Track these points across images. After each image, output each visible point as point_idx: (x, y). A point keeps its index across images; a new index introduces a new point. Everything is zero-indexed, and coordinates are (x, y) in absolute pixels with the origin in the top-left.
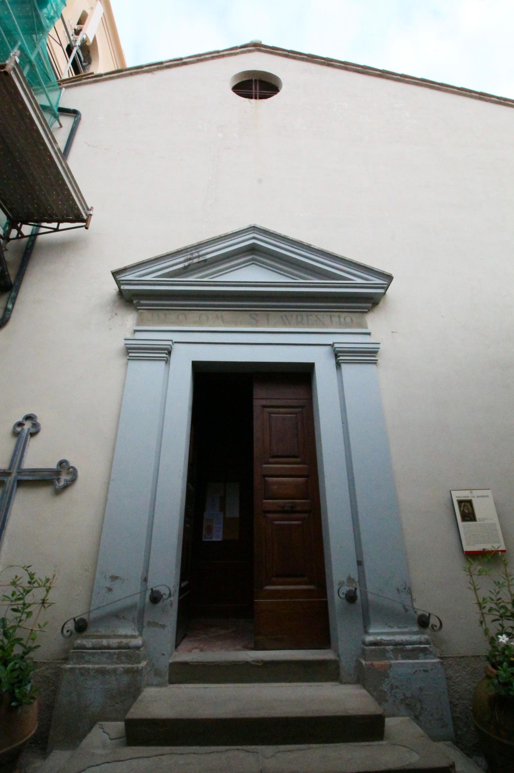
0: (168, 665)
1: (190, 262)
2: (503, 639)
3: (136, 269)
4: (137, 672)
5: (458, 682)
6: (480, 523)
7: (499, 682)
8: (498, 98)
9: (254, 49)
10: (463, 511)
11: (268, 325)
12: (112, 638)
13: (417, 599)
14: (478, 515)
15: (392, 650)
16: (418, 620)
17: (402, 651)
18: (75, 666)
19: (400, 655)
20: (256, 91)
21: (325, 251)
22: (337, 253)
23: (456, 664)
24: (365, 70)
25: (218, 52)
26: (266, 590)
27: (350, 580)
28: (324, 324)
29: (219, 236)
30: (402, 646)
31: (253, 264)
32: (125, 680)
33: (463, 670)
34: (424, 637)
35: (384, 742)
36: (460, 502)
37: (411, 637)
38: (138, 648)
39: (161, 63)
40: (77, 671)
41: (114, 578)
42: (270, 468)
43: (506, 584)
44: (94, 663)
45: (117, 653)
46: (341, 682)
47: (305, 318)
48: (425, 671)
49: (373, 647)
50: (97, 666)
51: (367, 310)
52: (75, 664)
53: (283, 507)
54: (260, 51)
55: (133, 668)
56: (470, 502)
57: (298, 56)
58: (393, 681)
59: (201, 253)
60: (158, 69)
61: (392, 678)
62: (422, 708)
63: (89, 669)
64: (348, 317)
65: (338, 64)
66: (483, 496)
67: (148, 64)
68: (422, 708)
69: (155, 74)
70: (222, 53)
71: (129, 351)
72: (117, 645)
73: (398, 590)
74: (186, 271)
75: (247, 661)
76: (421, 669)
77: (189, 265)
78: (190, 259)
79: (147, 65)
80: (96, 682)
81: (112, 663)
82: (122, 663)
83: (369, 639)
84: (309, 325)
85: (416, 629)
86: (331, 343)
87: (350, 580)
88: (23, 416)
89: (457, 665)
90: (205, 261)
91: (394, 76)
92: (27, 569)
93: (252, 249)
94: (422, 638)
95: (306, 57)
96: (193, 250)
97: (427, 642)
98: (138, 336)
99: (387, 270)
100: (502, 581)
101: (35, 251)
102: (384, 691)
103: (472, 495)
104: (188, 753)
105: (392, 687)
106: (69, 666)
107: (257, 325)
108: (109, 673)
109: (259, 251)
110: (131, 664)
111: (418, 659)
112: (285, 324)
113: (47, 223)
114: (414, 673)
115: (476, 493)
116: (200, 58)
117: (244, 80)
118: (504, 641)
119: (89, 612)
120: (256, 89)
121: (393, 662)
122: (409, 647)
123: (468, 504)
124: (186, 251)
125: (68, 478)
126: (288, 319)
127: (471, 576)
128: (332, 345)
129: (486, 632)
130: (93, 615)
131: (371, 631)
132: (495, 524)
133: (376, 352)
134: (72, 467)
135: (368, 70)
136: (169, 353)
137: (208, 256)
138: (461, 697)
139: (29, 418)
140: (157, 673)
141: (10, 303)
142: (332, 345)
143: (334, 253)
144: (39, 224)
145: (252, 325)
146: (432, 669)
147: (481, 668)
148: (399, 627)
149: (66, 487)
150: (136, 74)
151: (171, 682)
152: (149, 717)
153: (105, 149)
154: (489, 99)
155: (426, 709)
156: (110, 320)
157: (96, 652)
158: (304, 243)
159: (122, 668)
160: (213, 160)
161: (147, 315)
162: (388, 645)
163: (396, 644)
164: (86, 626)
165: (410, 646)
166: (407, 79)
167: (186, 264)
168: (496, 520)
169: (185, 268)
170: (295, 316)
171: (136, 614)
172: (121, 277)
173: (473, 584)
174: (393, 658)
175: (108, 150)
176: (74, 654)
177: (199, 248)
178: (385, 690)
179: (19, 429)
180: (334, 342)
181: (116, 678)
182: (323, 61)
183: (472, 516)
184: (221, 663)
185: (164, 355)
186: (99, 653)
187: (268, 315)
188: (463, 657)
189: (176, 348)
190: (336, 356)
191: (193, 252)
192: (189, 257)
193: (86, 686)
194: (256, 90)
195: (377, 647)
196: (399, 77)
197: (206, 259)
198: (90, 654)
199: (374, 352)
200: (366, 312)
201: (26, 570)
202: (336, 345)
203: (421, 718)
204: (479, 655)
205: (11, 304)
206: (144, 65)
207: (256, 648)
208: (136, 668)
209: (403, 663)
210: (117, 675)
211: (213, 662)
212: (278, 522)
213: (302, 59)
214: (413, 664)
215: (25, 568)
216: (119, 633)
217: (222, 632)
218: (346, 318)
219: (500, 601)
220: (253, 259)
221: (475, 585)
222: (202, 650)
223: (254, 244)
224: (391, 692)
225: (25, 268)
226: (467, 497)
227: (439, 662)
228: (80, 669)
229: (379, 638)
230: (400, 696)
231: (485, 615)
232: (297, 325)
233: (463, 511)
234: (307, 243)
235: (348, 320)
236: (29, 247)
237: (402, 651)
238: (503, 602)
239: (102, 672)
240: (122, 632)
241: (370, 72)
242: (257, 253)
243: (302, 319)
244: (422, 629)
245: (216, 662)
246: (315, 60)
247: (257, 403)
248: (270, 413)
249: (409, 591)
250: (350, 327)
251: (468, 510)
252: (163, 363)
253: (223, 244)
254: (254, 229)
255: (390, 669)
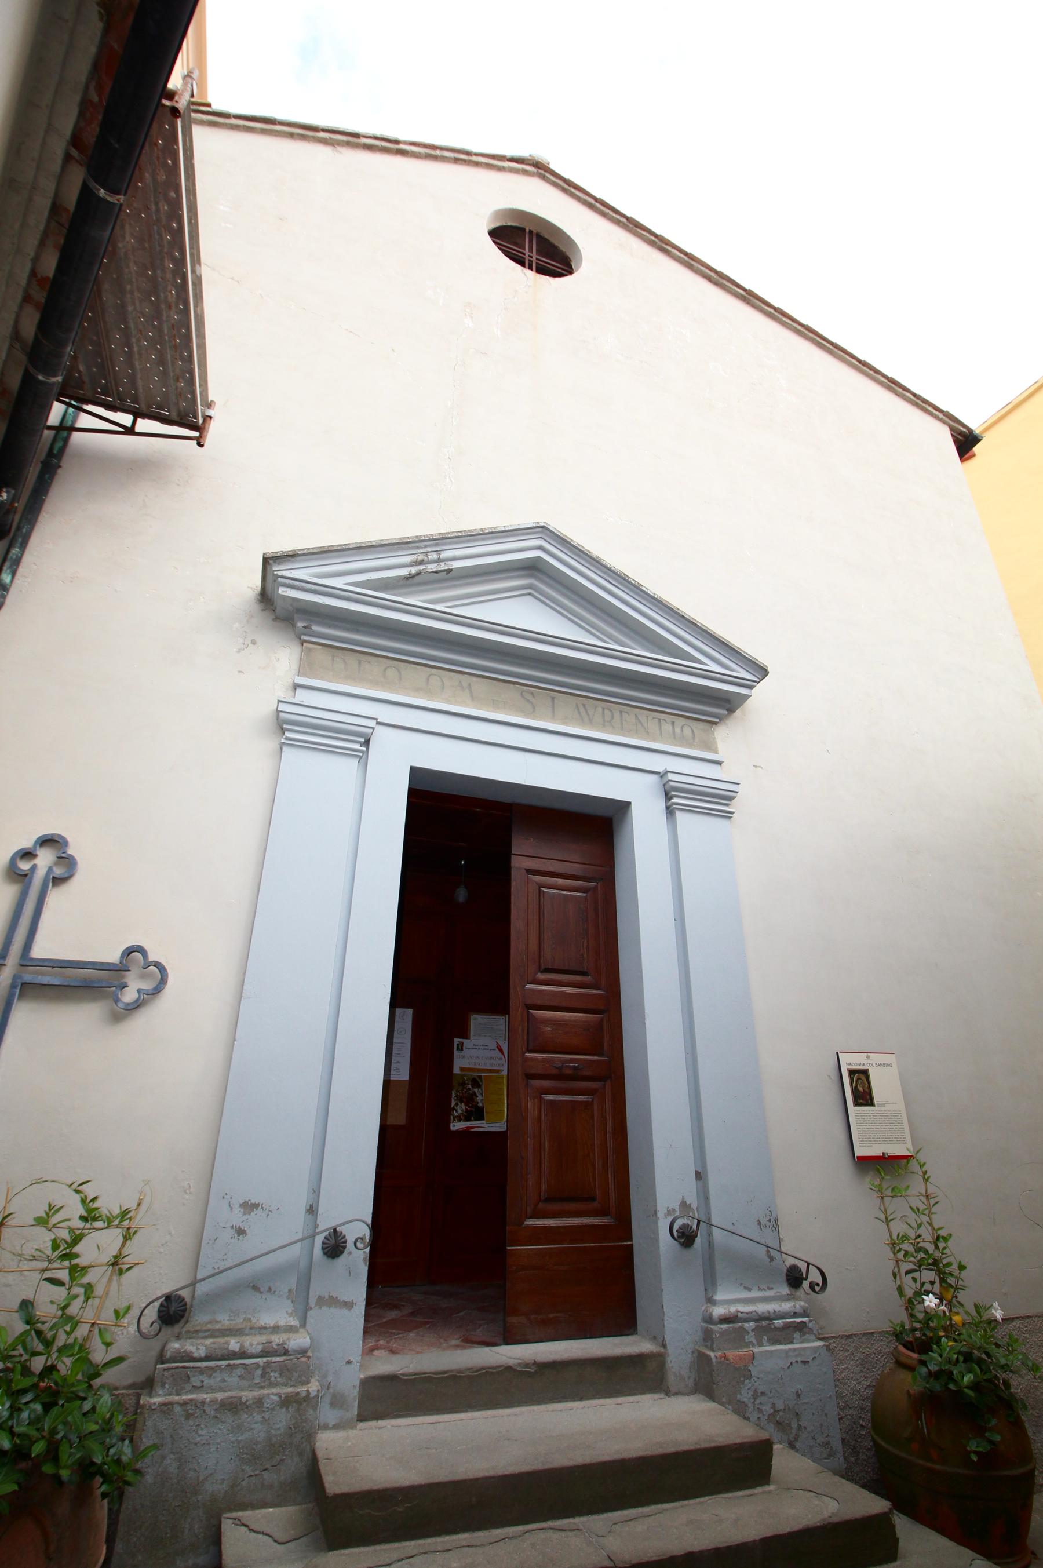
0: (357, 1383)
1: (422, 567)
2: (930, 1302)
3: (316, 559)
4: (308, 1401)
5: (843, 1378)
6: (879, 1109)
7: (930, 1371)
8: (914, 395)
9: (534, 173)
10: (856, 1087)
11: (553, 718)
12: (247, 1335)
13: (785, 1239)
14: (877, 1097)
15: (753, 1330)
16: (787, 1275)
17: (768, 1330)
18: (169, 1399)
19: (765, 1337)
20: (531, 255)
21: (664, 602)
22: (210, 429)
23: (841, 1349)
24: (721, 280)
25: (468, 153)
26: (528, 1227)
27: (684, 1205)
28: (647, 732)
29: (481, 530)
30: (768, 1322)
31: (530, 594)
32: (282, 1420)
33: (850, 1358)
34: (799, 1305)
35: (772, 1487)
36: (852, 1073)
37: (781, 1306)
38: (303, 1352)
39: (357, 135)
40: (177, 1409)
41: (249, 1207)
42: (541, 991)
43: (927, 1212)
44: (212, 1390)
45: (261, 1364)
46: (668, 1393)
47: (617, 715)
48: (805, 1362)
49: (725, 1326)
50: (220, 1396)
51: (718, 720)
52: (170, 1395)
53: (560, 1068)
54: (543, 178)
55: (298, 1394)
56: (865, 1073)
57: (611, 213)
58: (756, 1384)
59: (443, 555)
60: (348, 144)
61: (756, 1379)
62: (799, 1426)
63: (203, 1402)
64: (686, 728)
65: (678, 254)
66: (884, 1065)
67: (330, 128)
68: (799, 1426)
69: (340, 153)
70: (474, 158)
71: (285, 726)
72: (260, 1348)
73: (759, 1223)
74: (409, 582)
75: (509, 1365)
76: (799, 1360)
77: (419, 574)
78: (421, 562)
79: (327, 128)
80: (220, 1429)
81: (251, 1388)
82: (272, 1385)
83: (718, 1311)
84: (623, 730)
85: (785, 1290)
86: (660, 770)
87: (684, 1205)
88: (35, 837)
89: (842, 1350)
90: (449, 571)
91: (766, 307)
92: (80, 1188)
93: (533, 568)
94: (798, 1306)
95: (624, 220)
96: (430, 546)
97: (805, 1314)
98: (302, 696)
99: (762, 658)
100: (922, 1207)
101: (65, 462)
102: (744, 1402)
103: (869, 1062)
104: (458, 1548)
105: (755, 1396)
106: (157, 1400)
107: (532, 713)
108: (247, 1407)
109: (539, 570)
110: (291, 1386)
111: (792, 1343)
112: (582, 723)
113: (106, 410)
114: (789, 1367)
115: (875, 1058)
116: (431, 153)
117: (509, 224)
118: (933, 1305)
119: (193, 1284)
120: (531, 250)
121: (756, 1350)
122: (779, 1323)
123: (863, 1077)
124: (417, 544)
125: (147, 985)
126: (587, 712)
127: (882, 1198)
128: (661, 774)
129: (900, 1290)
130: (202, 1289)
131: (718, 1297)
132: (899, 1112)
133: (731, 799)
134: (157, 964)
135: (725, 282)
136: (367, 743)
137: (456, 565)
138: (848, 1405)
139: (48, 841)
140: (338, 1401)
141: (8, 571)
142: (662, 775)
143: (678, 609)
144: (80, 405)
145: (526, 715)
146: (814, 1358)
147: (875, 1354)
148: (760, 1289)
149: (137, 1006)
150: (300, 139)
151: (362, 1418)
152: (366, 1486)
153: (232, 279)
154: (901, 393)
155: (805, 1428)
156: (239, 651)
157: (217, 1366)
158: (629, 579)
159: (276, 1394)
160: (454, 369)
161: (321, 656)
162: (747, 1320)
163: (760, 1318)
164: (185, 1311)
165: (780, 1321)
166: (784, 319)
167: (414, 570)
168: (901, 1106)
169: (411, 577)
170: (600, 710)
171: (292, 1282)
172: (280, 570)
173: (885, 1212)
174: (756, 1343)
175: (238, 282)
176: (166, 1373)
177: (443, 544)
178: (745, 1400)
179: (24, 866)
180: (668, 770)
181: (263, 1417)
182: (653, 238)
183: (868, 1097)
184: (460, 1371)
185: (357, 747)
186: (223, 1367)
187: (553, 698)
188: (849, 1337)
189: (381, 737)
190: (668, 796)
191: (429, 549)
192: (421, 557)
193: (198, 1439)
194: (529, 251)
195: (731, 1325)
196: (772, 311)
197: (451, 568)
198: (201, 1371)
199: (728, 798)
200: (715, 723)
201: (77, 1191)
202: (671, 777)
203: (798, 1445)
204: (873, 1331)
205: (9, 574)
206: (321, 127)
207: (510, 1338)
208: (304, 1394)
209: (772, 1352)
210: (264, 1411)
211: (445, 1372)
212: (552, 1097)
213: (618, 223)
214: (787, 1352)
215: (74, 1186)
216: (262, 1323)
217: (392, 1314)
218: (684, 728)
219: (918, 1240)
220: (530, 587)
221: (888, 1214)
222: (392, 1352)
223: (539, 557)
224: (753, 1403)
225: (44, 497)
226: (861, 1064)
227: (824, 1345)
228: (184, 1404)
229: (733, 1309)
230: (767, 1409)
231: (900, 1263)
232: (604, 726)
233: (856, 1087)
234: (636, 581)
235: (687, 731)
236: (55, 451)
237: (768, 1330)
238: (924, 1241)
239: (233, 1407)
240: (267, 1319)
241: (728, 287)
242: (539, 575)
243: (613, 717)
244: (793, 1290)
245: (452, 1371)
246: (640, 233)
247: (519, 863)
248: (541, 886)
249: (774, 1224)
250: (691, 746)
251: (863, 1087)
252: (355, 762)
253: (645, 607)
254: (543, 530)
255: (752, 1363)
